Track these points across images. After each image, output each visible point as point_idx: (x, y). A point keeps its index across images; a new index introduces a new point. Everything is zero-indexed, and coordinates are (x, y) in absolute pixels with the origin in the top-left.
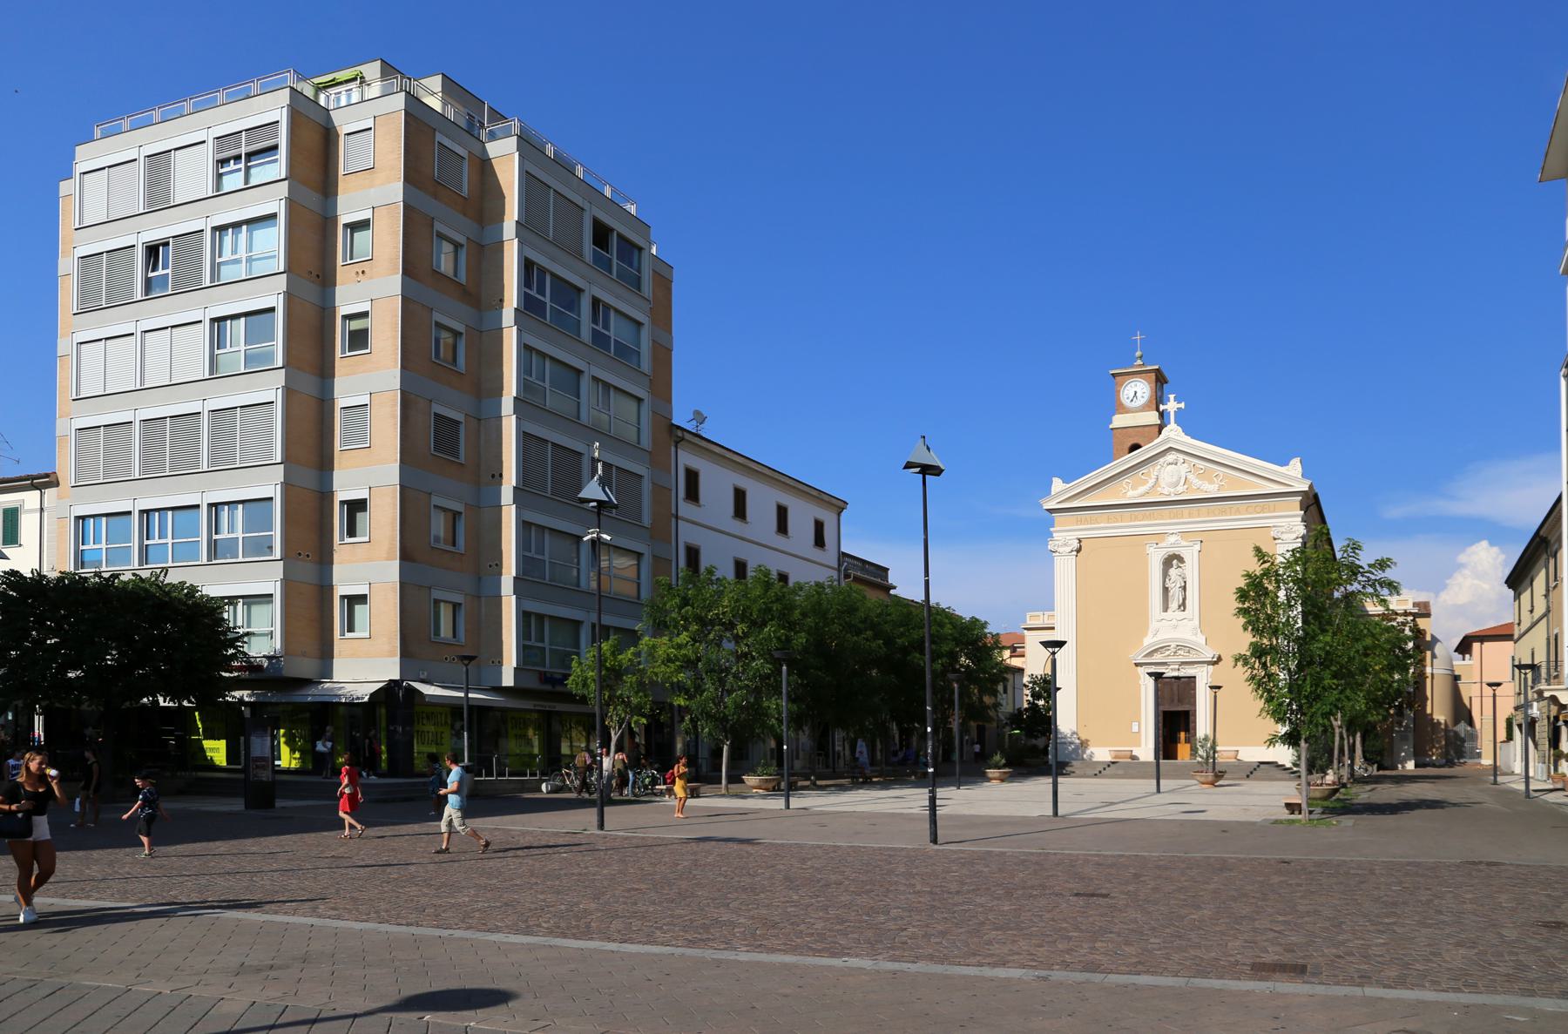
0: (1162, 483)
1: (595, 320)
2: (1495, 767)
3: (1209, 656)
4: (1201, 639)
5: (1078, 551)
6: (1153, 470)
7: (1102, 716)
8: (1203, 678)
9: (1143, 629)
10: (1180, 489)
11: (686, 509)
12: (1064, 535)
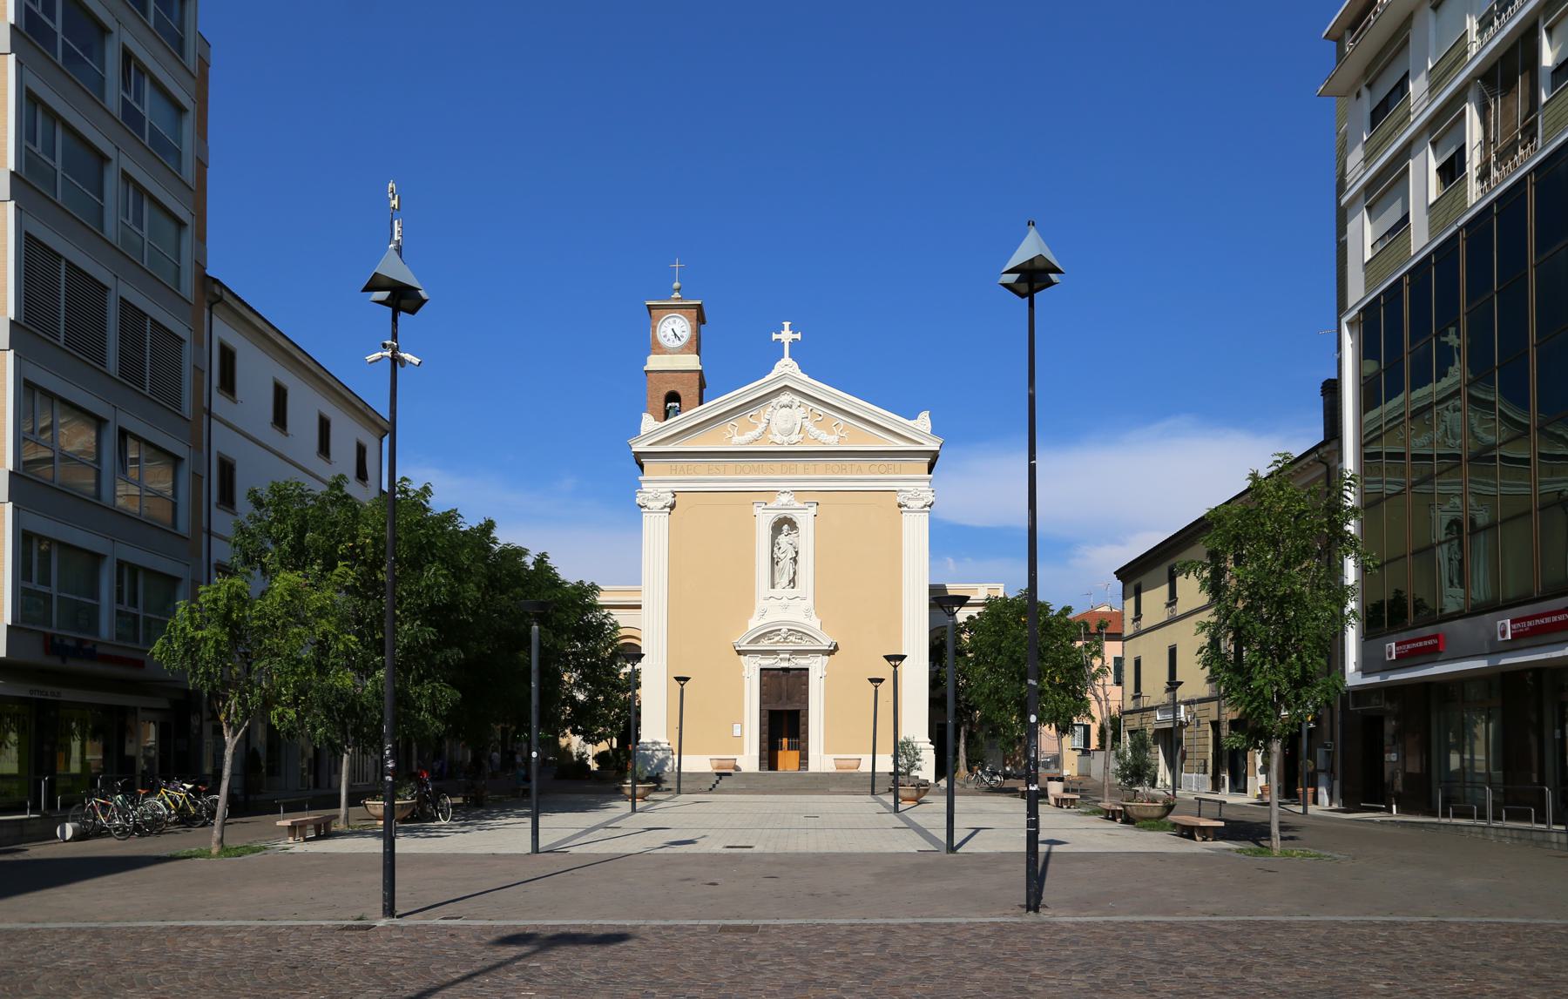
1: (126, 87)
2: (896, 774)
5: (672, 507)
6: (765, 412)
7: (693, 710)
8: (817, 668)
9: (746, 604)
10: (795, 438)
11: (220, 403)
12: (656, 486)
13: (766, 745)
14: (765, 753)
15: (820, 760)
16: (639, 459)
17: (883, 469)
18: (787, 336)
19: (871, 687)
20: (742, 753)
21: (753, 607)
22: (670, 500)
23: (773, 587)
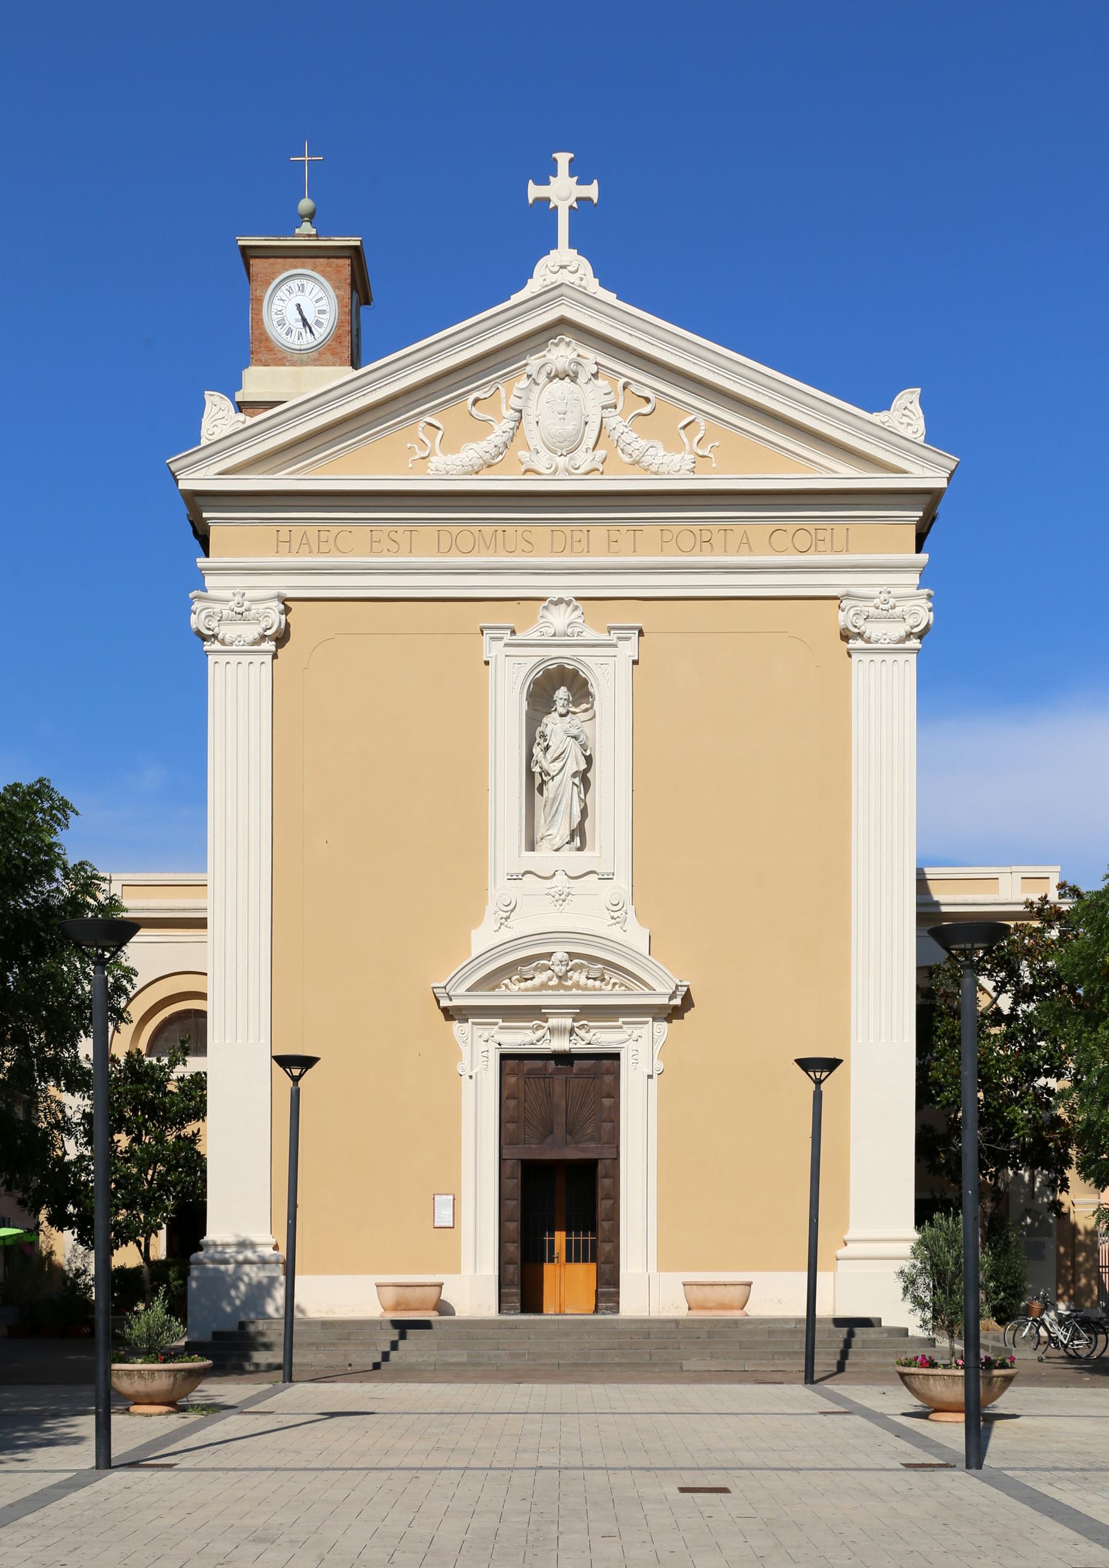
0: (532, 434)
3: (661, 994)
4: (635, 936)
5: (282, 638)
6: (509, 391)
9: (469, 897)
12: (239, 584)
13: (514, 1249)
14: (513, 1270)
15: (651, 1286)
16: (198, 515)
17: (803, 540)
18: (563, 190)
19: (804, 1083)
20: (456, 1269)
21: (484, 901)
22: (274, 619)
23: (531, 846)
